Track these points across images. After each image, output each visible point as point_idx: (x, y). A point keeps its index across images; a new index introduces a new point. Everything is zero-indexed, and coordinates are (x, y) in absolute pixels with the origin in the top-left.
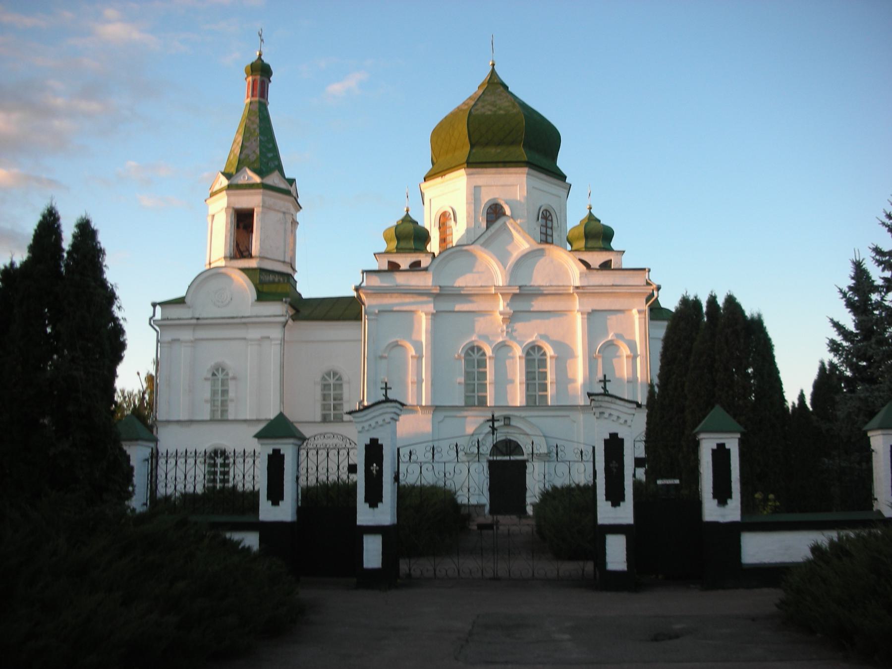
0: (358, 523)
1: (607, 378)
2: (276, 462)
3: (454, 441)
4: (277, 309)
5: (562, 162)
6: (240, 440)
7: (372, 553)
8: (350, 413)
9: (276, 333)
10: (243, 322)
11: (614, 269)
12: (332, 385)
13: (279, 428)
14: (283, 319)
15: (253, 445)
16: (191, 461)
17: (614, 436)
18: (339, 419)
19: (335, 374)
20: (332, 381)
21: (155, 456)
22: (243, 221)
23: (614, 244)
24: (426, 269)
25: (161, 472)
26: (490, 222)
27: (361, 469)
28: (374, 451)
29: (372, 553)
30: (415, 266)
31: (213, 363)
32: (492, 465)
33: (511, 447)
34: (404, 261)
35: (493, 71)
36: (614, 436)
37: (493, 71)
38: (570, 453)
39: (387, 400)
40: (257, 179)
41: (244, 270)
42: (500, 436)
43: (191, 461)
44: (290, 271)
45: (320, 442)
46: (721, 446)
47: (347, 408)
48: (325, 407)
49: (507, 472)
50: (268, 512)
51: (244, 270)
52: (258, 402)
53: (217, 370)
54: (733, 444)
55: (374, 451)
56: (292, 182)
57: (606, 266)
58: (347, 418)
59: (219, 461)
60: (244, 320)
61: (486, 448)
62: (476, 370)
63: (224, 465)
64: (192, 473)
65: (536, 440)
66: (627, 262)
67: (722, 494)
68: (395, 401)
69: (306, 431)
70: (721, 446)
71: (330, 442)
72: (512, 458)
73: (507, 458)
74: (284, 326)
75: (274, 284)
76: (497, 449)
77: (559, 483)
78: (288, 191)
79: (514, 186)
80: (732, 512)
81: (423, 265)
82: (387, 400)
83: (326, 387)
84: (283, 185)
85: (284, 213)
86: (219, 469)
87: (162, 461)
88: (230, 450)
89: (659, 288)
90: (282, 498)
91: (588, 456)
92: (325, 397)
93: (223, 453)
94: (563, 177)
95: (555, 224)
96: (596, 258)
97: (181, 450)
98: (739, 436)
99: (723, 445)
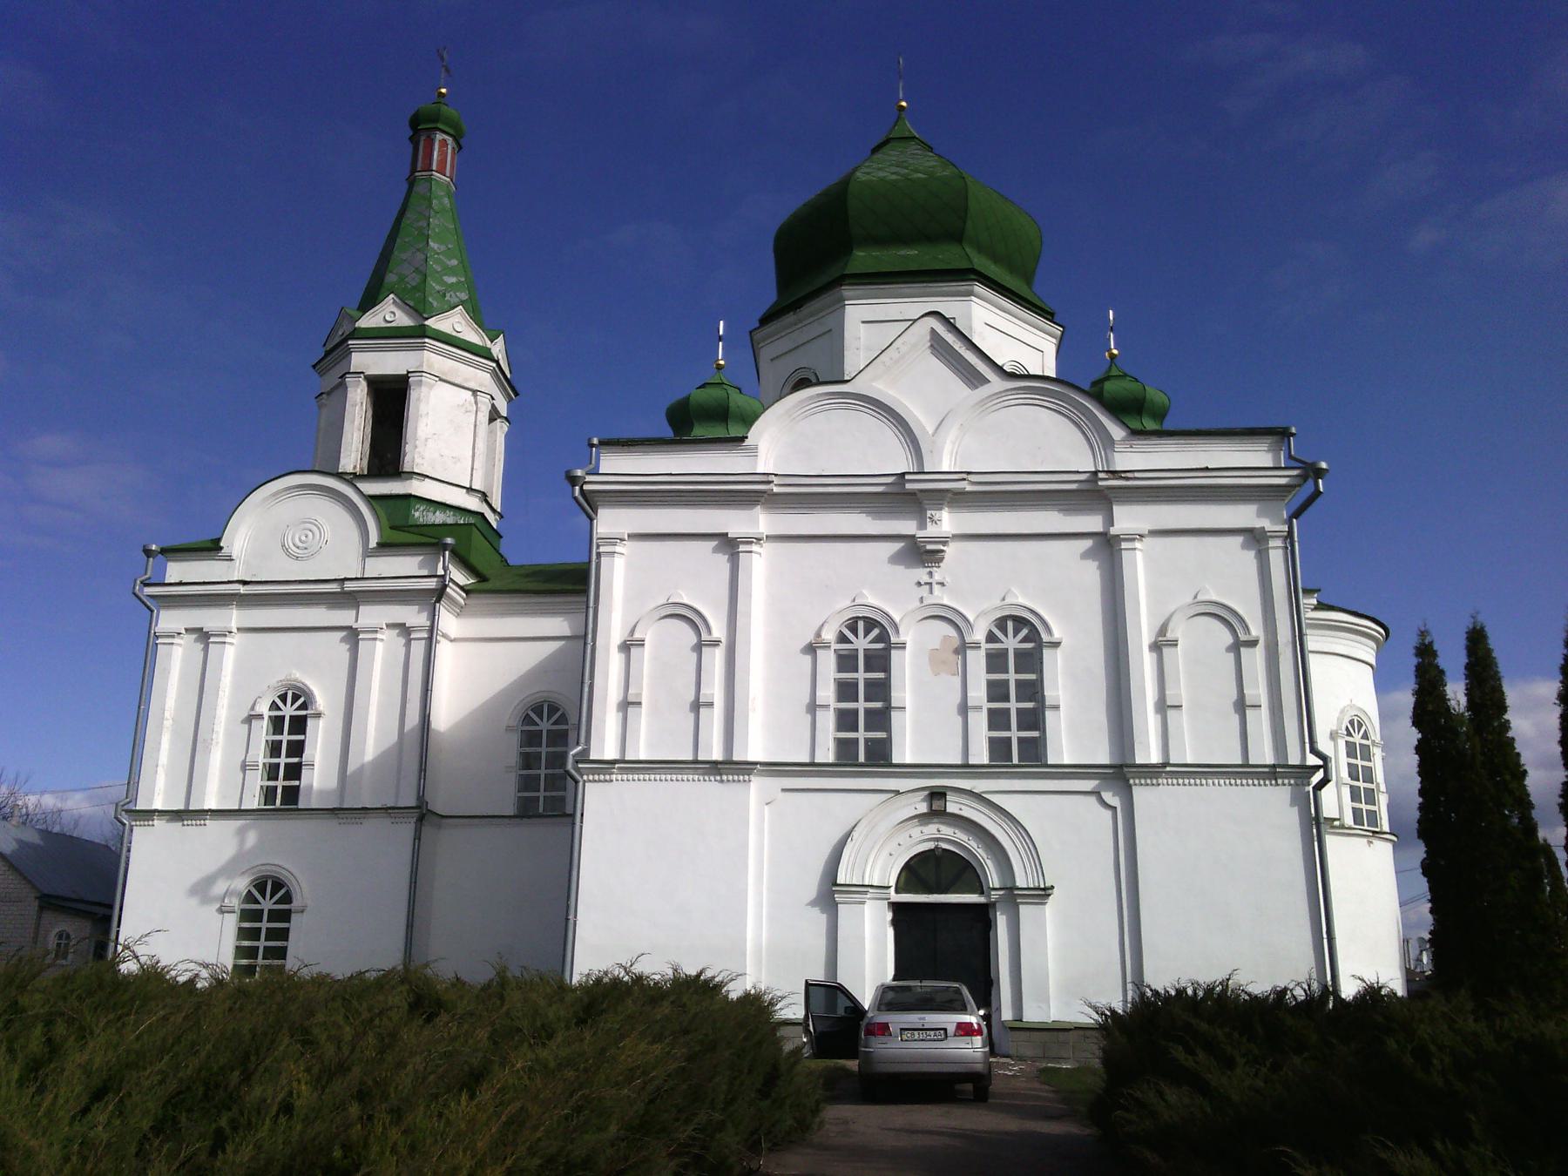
10: (346, 596)
14: (432, 584)
20: (545, 726)
31: (273, 682)
32: (903, 916)
41: (372, 499)
53: (296, 698)
60: (349, 586)
74: (438, 601)
76: (919, 871)
85: (475, 392)
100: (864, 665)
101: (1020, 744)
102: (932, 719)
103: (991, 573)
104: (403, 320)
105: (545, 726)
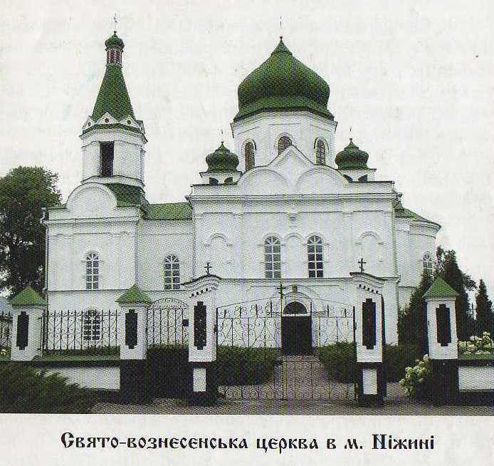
0: (190, 361)
1: (364, 261)
2: (131, 319)
3: (255, 302)
4: (132, 213)
5: (332, 106)
6: (104, 303)
7: (199, 382)
8: (183, 285)
9: (131, 229)
10: (107, 222)
11: (370, 182)
12: (171, 268)
13: (132, 297)
15: (115, 307)
16: (72, 319)
17: (369, 301)
18: (177, 287)
19: (174, 257)
20: (172, 262)
21: (46, 316)
22: (107, 151)
23: (370, 164)
24: (236, 184)
25: (50, 326)
26: (280, 150)
27: (192, 322)
28: (200, 310)
29: (199, 382)
30: (229, 182)
33: (296, 307)
34: (221, 178)
35: (281, 41)
36: (369, 301)
37: (281, 41)
38: (337, 311)
39: (209, 275)
40: (113, 121)
41: (108, 185)
42: (290, 300)
43: (72, 319)
44: (141, 186)
45: (163, 304)
46: (443, 306)
47: (182, 282)
48: (168, 280)
49: (297, 329)
50: (127, 354)
51: (108, 185)
52: (117, 276)
53: (90, 255)
54: (15, 350)
55: (200, 310)
56: (140, 122)
57: (363, 180)
58: (182, 288)
59: (92, 319)
61: (279, 308)
62: (316, 261)
63: (95, 322)
64: (73, 327)
65: (315, 302)
66: (377, 177)
67: (444, 339)
68: (215, 276)
69: (153, 298)
70: (443, 306)
71: (170, 304)
72: (297, 315)
73: (294, 315)
75: (129, 194)
77: (239, 343)
78: (138, 130)
79: (301, 127)
80: (449, 353)
81: (234, 180)
82: (209, 275)
83: (168, 266)
84: (133, 125)
86: (92, 325)
87: (51, 319)
88: (99, 310)
89: (401, 196)
90: (136, 343)
91: (350, 313)
92: (167, 274)
93: (95, 313)
94: (330, 117)
95: (327, 151)
96: (355, 175)
97: (65, 311)
98: (455, 299)
99: (444, 305)
100: (272, 249)
101: (316, 267)
102: (294, 265)
103: (307, 228)
104: (113, 121)
105: (172, 262)
